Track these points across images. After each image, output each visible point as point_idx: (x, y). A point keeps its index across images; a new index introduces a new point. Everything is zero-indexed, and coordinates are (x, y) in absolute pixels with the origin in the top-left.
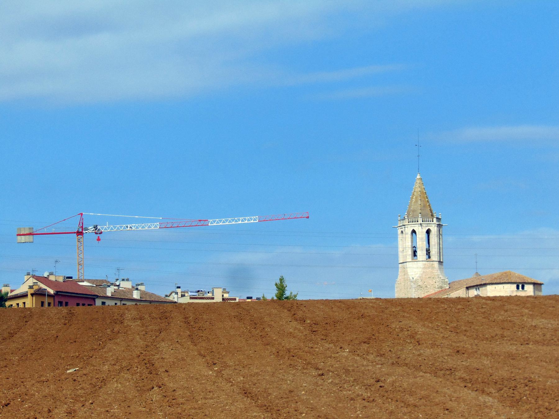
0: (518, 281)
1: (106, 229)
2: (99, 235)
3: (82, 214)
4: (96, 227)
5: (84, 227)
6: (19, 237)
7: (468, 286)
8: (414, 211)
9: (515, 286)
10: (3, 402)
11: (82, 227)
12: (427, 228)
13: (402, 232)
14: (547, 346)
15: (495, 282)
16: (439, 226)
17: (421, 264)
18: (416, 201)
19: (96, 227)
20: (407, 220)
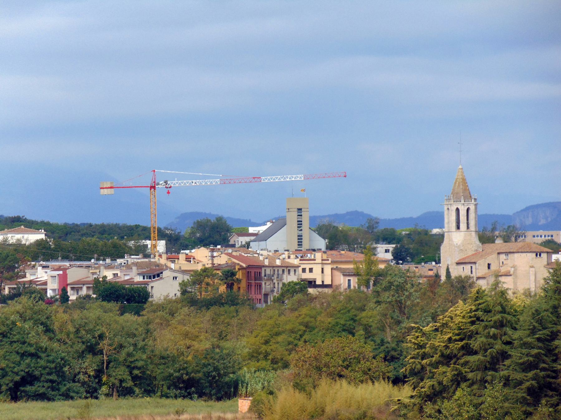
0: (537, 250)
1: (174, 184)
2: (169, 189)
3: (154, 171)
4: (166, 182)
5: (156, 182)
6: (102, 190)
7: (499, 252)
8: (457, 193)
9: (535, 254)
10: (43, 344)
11: (154, 182)
12: (467, 207)
13: (448, 209)
14: (93, 393)
15: (520, 251)
16: (476, 205)
17: (462, 234)
18: (459, 185)
19: (166, 182)
20: (452, 201)
